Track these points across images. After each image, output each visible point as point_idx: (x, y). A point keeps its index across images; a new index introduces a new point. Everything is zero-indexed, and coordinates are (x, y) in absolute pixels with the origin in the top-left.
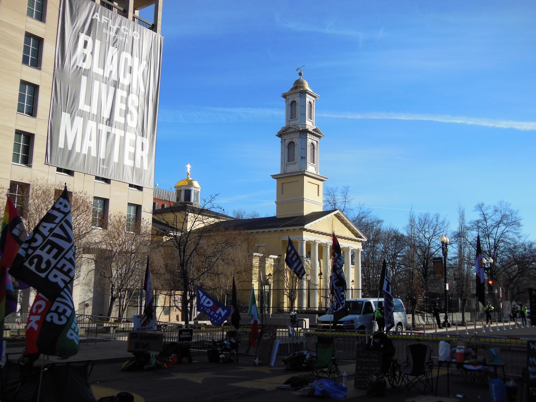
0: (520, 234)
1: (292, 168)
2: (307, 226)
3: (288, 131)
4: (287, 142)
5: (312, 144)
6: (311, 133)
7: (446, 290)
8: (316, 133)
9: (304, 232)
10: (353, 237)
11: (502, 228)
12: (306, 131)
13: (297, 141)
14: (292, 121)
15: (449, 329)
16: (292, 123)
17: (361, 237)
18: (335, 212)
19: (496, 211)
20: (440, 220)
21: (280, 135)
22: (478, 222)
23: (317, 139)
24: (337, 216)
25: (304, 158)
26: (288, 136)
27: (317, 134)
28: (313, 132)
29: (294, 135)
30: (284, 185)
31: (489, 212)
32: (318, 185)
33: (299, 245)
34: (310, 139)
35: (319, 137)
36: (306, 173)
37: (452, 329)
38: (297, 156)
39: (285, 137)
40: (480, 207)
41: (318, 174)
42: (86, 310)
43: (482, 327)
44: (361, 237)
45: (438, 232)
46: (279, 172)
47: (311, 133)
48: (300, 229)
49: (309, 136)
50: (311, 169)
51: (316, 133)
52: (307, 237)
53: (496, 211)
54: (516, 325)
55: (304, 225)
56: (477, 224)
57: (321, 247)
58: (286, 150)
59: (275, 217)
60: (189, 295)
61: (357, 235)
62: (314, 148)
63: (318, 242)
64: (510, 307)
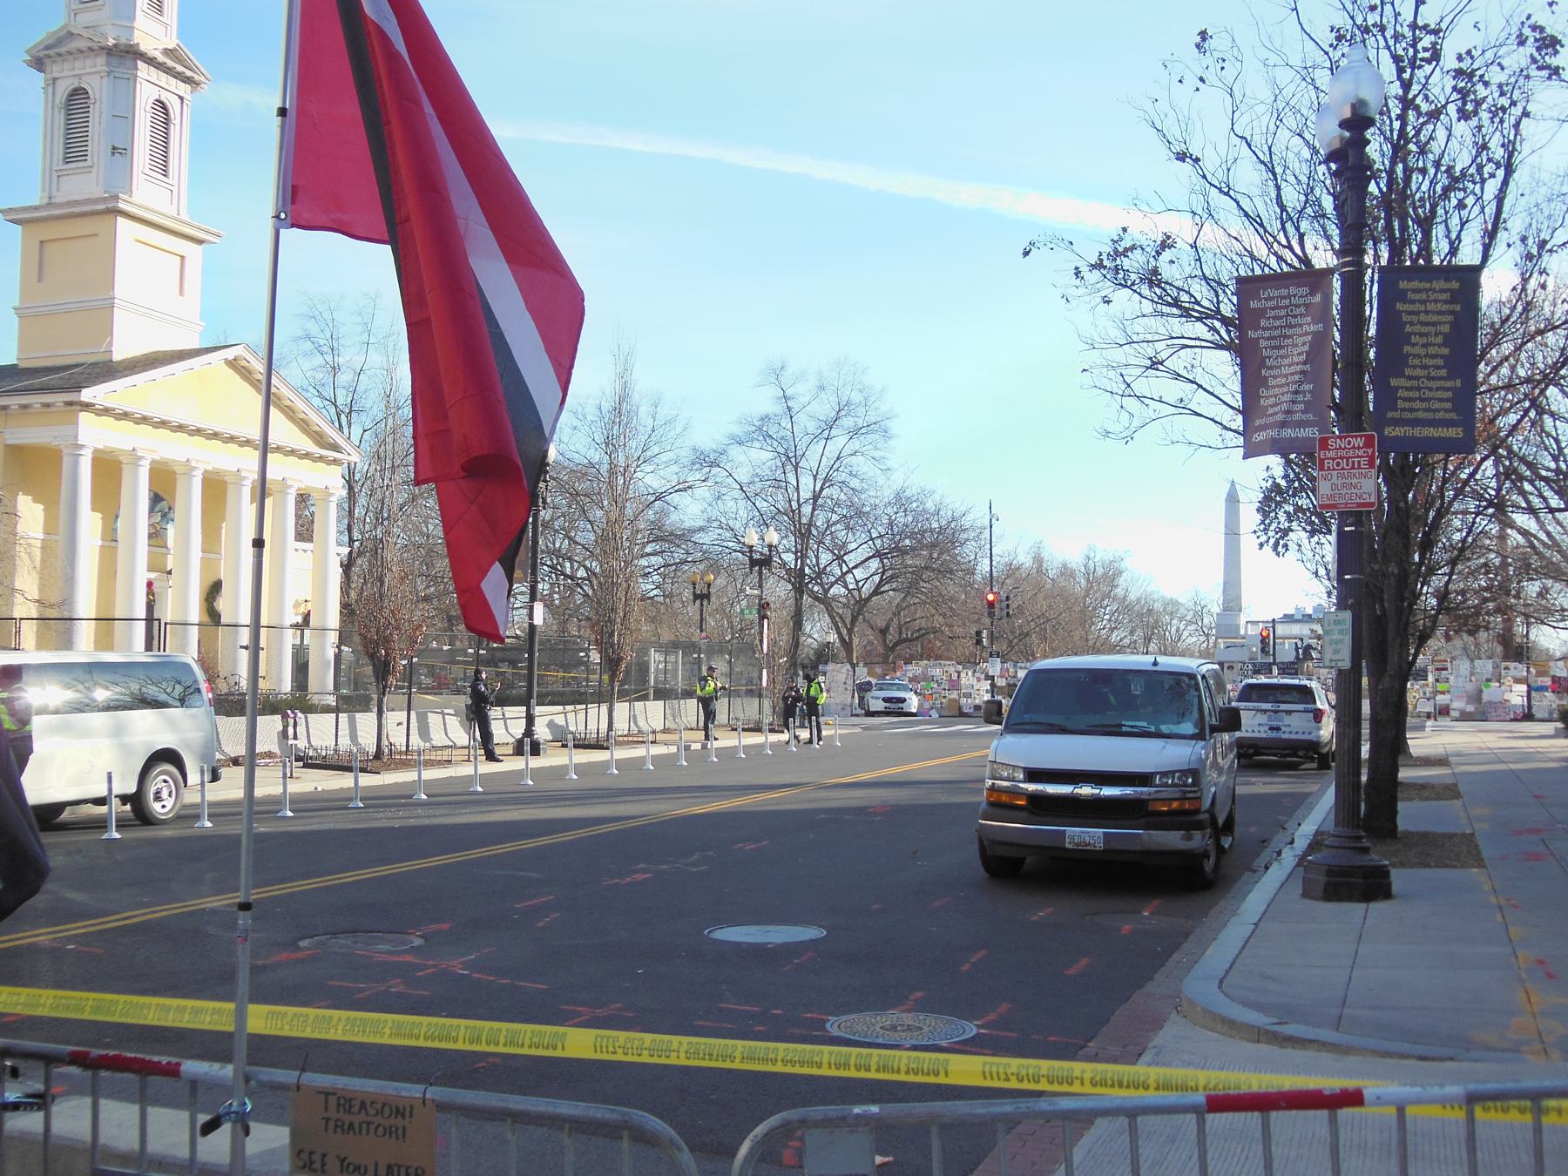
0: (889, 464)
1: (82, 186)
2: (86, 395)
3: (63, 50)
4: (64, 88)
5: (162, 106)
6: (151, 61)
7: (532, 627)
8: (174, 65)
9: (85, 417)
10: (307, 445)
11: (839, 442)
12: (127, 55)
13: (98, 87)
14: (84, 11)
15: (535, 763)
16: (85, 18)
17: (335, 448)
18: (230, 354)
19: (822, 388)
20: (663, 414)
21: (38, 63)
22: (765, 418)
23: (183, 89)
24: (233, 364)
25: (122, 151)
26: (67, 66)
27: (180, 68)
28: (161, 58)
29: (88, 62)
30: (49, 248)
31: (802, 392)
32: (183, 257)
33: (66, 461)
34: (149, 86)
35: (188, 80)
36: (122, 205)
37: (621, 754)
38: (97, 143)
39: (55, 70)
40: (777, 372)
41: (184, 216)
42: (518, 729)
43: (673, 749)
44: (335, 448)
45: (656, 449)
46: (34, 197)
47: (151, 61)
48: (70, 404)
49: (143, 69)
50: (145, 193)
51: (174, 65)
52: (93, 433)
53: (822, 388)
54: (793, 742)
55: (78, 388)
56: (761, 431)
57: (216, 488)
58: (60, 118)
59: (14, 366)
60: (1318, 715)
61: (319, 438)
62: (167, 122)
63: (202, 467)
64: (850, 682)
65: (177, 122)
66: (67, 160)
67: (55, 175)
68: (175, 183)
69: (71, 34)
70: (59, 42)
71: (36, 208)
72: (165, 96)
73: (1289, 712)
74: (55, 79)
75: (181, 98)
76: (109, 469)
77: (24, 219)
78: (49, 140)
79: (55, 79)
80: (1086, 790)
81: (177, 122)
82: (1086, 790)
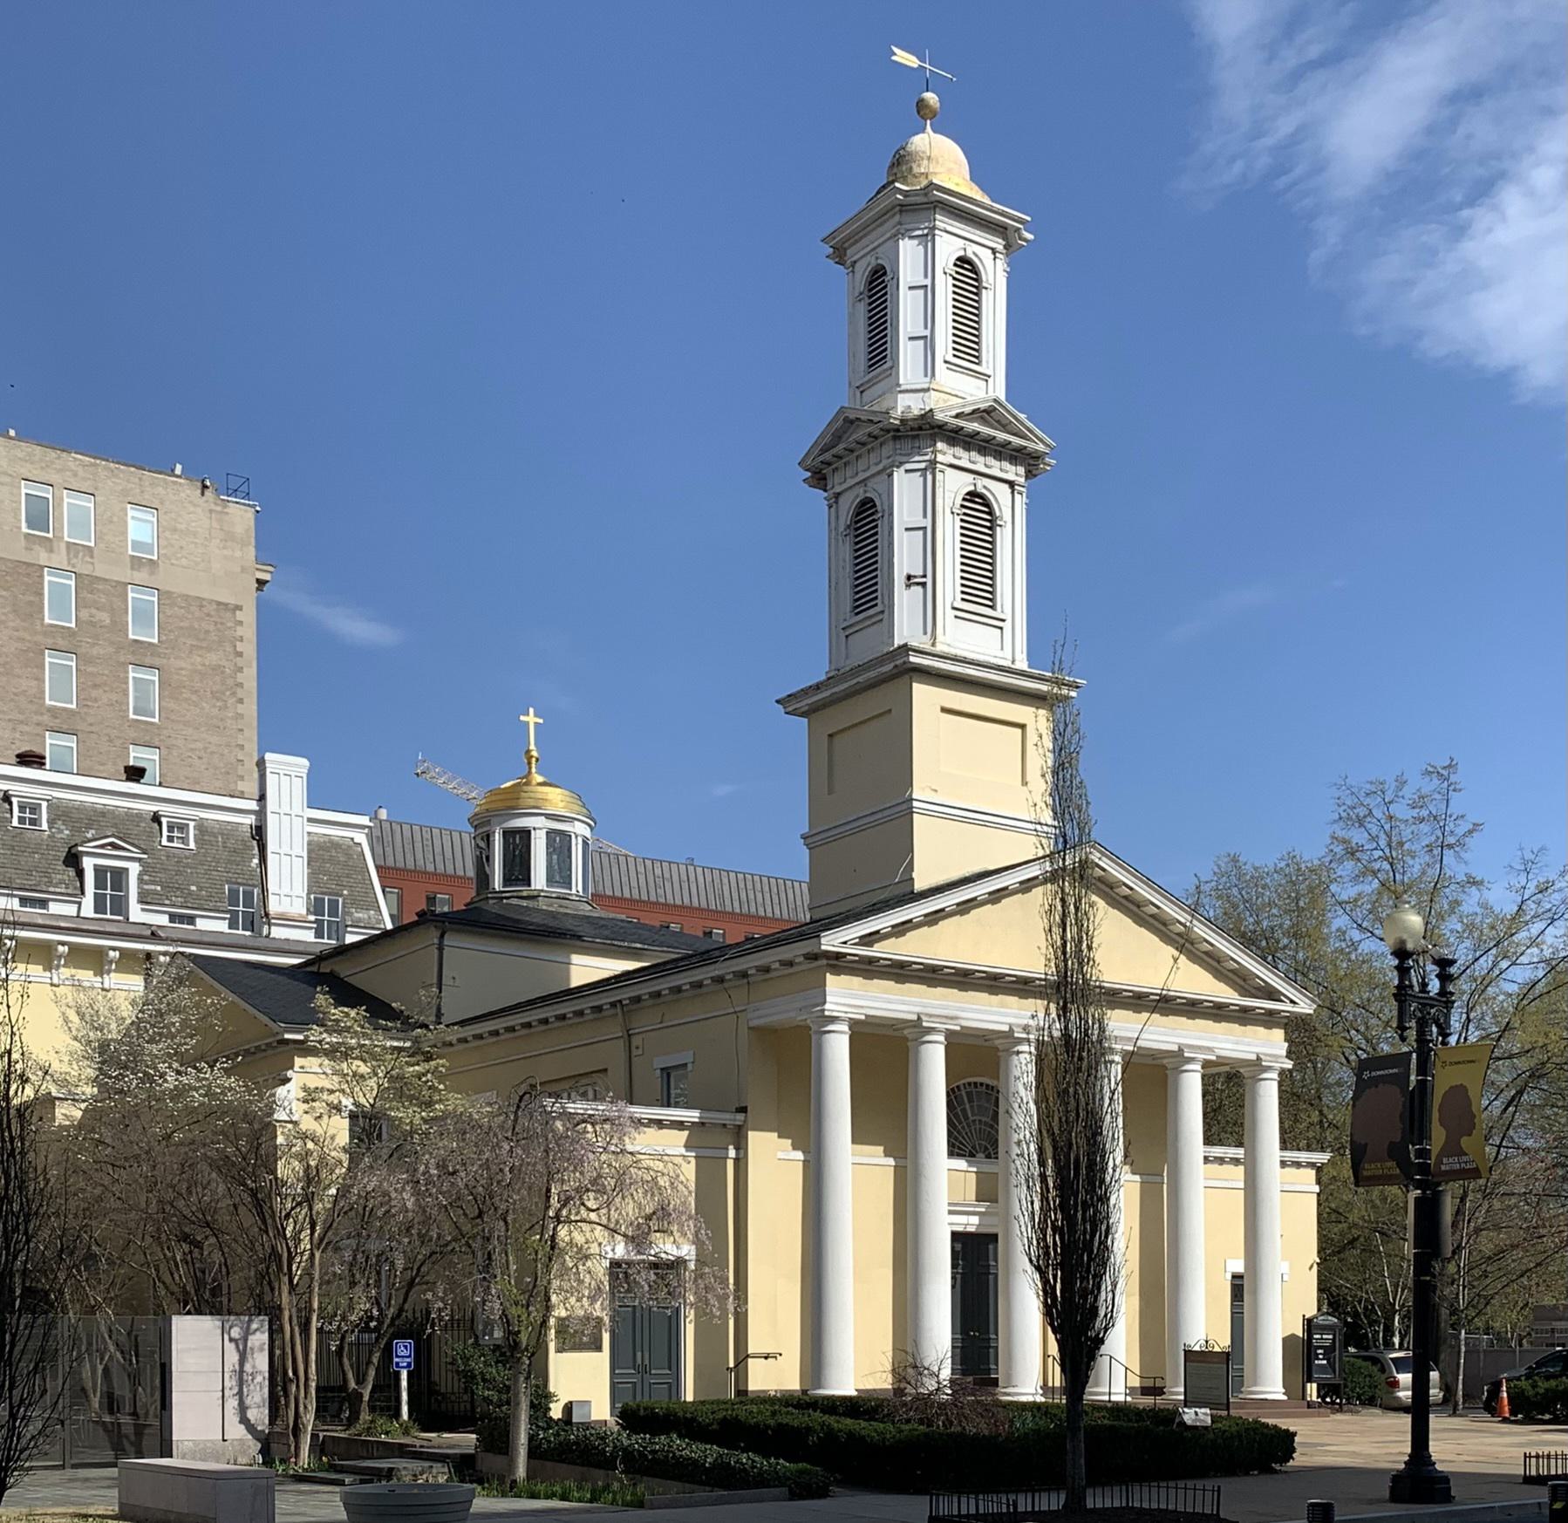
4: (848, 504)
10: (1225, 994)
17: (1272, 994)
27: (1002, 436)
57: (976, 1058)
65: (1007, 515)
66: (857, 609)
67: (843, 635)
68: (1009, 618)
69: (850, 423)
70: (837, 437)
71: (818, 687)
72: (982, 485)
73: (639, 1123)
74: (837, 496)
75: (1011, 484)
76: (885, 1052)
77: (797, 703)
78: (833, 586)
79: (837, 496)
80: (313, 1356)
81: (1007, 515)
82: (313, 1356)
